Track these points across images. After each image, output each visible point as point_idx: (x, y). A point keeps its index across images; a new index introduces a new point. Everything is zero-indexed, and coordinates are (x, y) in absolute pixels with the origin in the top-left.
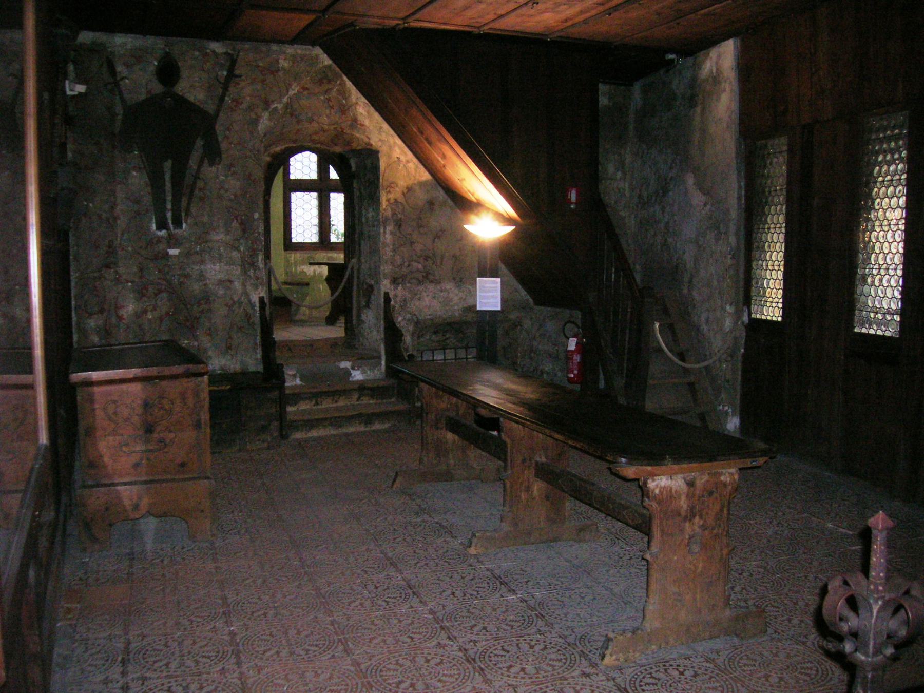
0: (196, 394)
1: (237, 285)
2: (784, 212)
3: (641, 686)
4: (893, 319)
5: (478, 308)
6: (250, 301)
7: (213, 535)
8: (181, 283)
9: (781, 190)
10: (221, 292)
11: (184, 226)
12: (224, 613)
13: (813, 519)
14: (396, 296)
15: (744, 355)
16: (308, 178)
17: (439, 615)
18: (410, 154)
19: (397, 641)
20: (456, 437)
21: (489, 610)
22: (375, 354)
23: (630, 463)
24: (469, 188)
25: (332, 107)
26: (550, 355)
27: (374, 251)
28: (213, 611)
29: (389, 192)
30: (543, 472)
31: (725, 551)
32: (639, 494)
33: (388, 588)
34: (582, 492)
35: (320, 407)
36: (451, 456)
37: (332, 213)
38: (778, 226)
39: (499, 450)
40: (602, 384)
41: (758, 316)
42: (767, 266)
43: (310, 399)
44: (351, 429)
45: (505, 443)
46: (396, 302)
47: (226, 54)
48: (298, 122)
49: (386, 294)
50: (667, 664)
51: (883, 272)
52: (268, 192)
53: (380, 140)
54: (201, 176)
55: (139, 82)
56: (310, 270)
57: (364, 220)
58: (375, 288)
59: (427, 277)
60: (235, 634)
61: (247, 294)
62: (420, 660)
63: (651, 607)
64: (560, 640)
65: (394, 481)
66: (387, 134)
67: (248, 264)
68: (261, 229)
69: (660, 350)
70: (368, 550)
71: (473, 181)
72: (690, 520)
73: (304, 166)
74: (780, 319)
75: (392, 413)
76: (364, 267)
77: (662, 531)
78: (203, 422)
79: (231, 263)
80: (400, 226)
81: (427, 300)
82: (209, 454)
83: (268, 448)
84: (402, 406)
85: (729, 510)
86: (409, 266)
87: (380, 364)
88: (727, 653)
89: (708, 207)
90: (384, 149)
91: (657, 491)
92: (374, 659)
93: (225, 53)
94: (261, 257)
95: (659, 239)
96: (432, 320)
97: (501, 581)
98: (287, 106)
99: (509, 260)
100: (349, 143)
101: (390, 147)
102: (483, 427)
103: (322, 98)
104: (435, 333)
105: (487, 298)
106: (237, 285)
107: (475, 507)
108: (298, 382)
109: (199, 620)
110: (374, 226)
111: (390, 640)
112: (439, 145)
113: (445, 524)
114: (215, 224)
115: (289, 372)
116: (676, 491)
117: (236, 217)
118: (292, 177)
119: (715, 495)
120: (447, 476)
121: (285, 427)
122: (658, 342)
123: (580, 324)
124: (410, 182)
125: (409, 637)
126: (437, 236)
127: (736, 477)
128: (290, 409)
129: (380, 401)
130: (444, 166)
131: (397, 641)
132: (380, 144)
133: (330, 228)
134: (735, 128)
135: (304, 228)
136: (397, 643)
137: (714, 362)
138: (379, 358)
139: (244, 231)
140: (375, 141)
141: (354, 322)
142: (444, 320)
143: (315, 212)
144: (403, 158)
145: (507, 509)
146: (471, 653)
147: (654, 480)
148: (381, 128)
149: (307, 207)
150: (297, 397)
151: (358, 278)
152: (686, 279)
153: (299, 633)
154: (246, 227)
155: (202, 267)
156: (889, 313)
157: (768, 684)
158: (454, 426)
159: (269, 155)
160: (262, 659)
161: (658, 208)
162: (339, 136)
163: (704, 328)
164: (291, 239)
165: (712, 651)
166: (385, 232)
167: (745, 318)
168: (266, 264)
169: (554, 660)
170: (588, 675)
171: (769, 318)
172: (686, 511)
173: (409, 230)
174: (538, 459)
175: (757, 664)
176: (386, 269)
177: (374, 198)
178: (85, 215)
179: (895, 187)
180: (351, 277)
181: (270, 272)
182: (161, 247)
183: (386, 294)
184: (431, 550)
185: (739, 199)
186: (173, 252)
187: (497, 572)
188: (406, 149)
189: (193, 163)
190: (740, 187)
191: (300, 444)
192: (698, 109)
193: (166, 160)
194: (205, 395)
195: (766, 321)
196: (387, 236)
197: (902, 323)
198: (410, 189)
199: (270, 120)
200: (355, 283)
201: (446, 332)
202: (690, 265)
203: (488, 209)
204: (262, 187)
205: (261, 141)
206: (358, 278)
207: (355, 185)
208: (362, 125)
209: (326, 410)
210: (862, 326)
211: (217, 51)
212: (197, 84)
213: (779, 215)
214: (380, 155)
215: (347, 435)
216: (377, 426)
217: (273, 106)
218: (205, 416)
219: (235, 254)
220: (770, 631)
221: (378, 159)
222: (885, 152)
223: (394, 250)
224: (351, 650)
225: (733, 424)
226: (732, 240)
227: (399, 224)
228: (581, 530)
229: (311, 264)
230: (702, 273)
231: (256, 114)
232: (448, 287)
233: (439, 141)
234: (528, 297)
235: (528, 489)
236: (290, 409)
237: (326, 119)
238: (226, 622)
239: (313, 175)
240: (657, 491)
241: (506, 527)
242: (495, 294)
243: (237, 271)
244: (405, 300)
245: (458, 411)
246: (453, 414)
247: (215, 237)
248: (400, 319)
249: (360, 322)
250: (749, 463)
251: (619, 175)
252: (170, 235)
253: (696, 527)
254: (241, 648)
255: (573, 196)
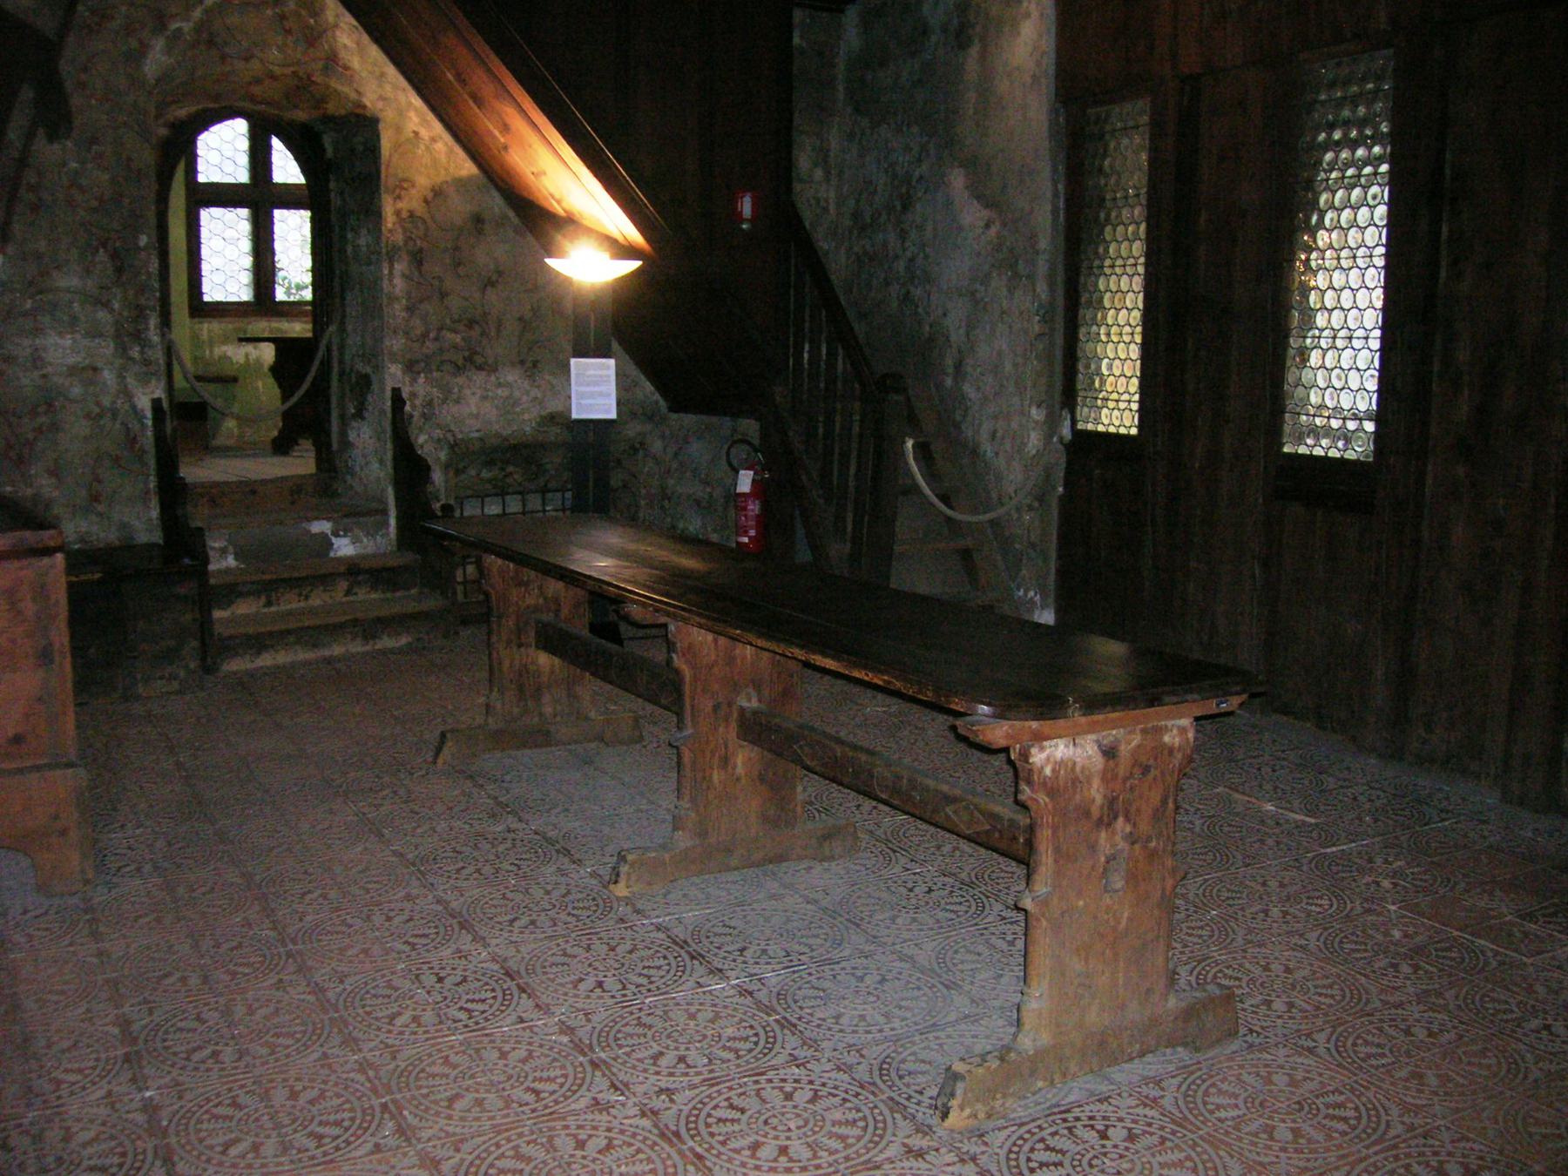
0: (41, 591)
1: (108, 376)
2: (1143, 236)
3: (756, 1035)
4: (1360, 429)
5: (575, 416)
6: (134, 407)
7: (87, 882)
9: (1137, 195)
10: (77, 391)
12: (127, 1058)
13: (1237, 796)
14: (414, 395)
15: (1061, 498)
16: (233, 181)
17: (583, 1034)
18: (438, 127)
19: (508, 1102)
20: (557, 661)
21: (679, 1016)
22: (374, 505)
23: (1000, 715)
24: (552, 190)
25: (288, 32)
26: (698, 503)
27: (373, 310)
28: (103, 1056)
29: (399, 197)
30: (754, 729)
31: (1170, 882)
32: (1011, 774)
33: (465, 980)
34: (849, 773)
35: (273, 609)
36: (546, 698)
37: (278, 246)
38: (1131, 261)
39: (665, 690)
40: (803, 555)
41: (1090, 427)
42: (1108, 335)
43: (256, 594)
44: (337, 650)
45: (677, 672)
46: (413, 407)
48: (223, 58)
49: (396, 393)
50: (1069, 1116)
51: (1340, 343)
52: (163, 199)
53: (382, 98)
56: (238, 354)
57: (349, 249)
58: (374, 378)
59: (472, 361)
60: (157, 1108)
61: (129, 396)
62: (565, 1144)
63: (1034, 1005)
64: (841, 1076)
65: (438, 751)
66: (396, 87)
67: (129, 334)
68: (154, 266)
69: (916, 489)
70: (408, 898)
71: (565, 179)
72: (1109, 825)
73: (223, 151)
74: (1134, 431)
75: (414, 617)
76: (353, 341)
77: (1057, 850)
78: (57, 646)
79: (94, 333)
80: (420, 263)
81: (472, 404)
82: (71, 710)
83: (179, 692)
84: (433, 603)
85: (1175, 801)
86: (436, 339)
87: (387, 524)
88: (1175, 1081)
89: (993, 230)
90: (388, 116)
91: (1048, 771)
92: (466, 1147)
94: (153, 321)
95: (895, 289)
96: (481, 439)
97: (690, 951)
98: (200, 27)
99: (625, 325)
100: (320, 102)
101: (401, 113)
102: (602, 637)
103: (269, 12)
104: (490, 463)
105: (592, 395)
106: (108, 376)
107: (615, 796)
108: (231, 561)
109: (72, 1077)
110: (369, 264)
111: (492, 1099)
112: (498, 105)
113: (550, 834)
115: (215, 543)
116: (1083, 768)
117: (104, 245)
118: (202, 179)
119: (1153, 772)
120: (541, 737)
121: (212, 649)
122: (913, 479)
123: (756, 442)
124: (439, 180)
125: (528, 1089)
126: (491, 283)
127: (1191, 735)
128: (218, 614)
129: (389, 595)
130: (506, 148)
131: (508, 1102)
132: (380, 105)
133: (274, 275)
134: (1047, 86)
135: (225, 268)
136: (508, 1107)
137: (1008, 514)
138: (385, 512)
139: (119, 270)
140: (370, 100)
141: (335, 446)
142: (506, 439)
143: (246, 245)
144: (424, 133)
145: (685, 804)
146: (668, 1118)
147: (1042, 749)
148: (383, 75)
149: (229, 233)
150: (231, 591)
151: (341, 362)
152: (949, 362)
153: (294, 1095)
154: (121, 264)
156: (1355, 417)
157: (1276, 1146)
158: (553, 640)
159: (165, 125)
160: (221, 1164)
161: (892, 237)
162: (302, 88)
163: (987, 448)
164: (201, 294)
165: (1146, 1080)
166: (391, 273)
167: (1066, 432)
168: (163, 335)
169: (840, 1123)
170: (920, 1154)
171: (1112, 429)
172: (1102, 807)
173: (437, 270)
174: (745, 704)
175: (1240, 1102)
176: (395, 343)
177: (372, 212)
179: (1366, 188)
180: (326, 365)
181: (170, 350)
183: (396, 393)
184: (537, 893)
185: (1055, 212)
187: (679, 932)
188: (430, 116)
190: (1056, 195)
191: (245, 683)
192: (974, 51)
194: (60, 596)
195: (1107, 435)
196: (396, 280)
197: (1378, 436)
198: (438, 192)
199: (168, 51)
200: (336, 370)
201: (508, 462)
202: (957, 336)
203: (589, 231)
204: (150, 187)
205: (150, 93)
206: (341, 362)
207: (332, 185)
208: (346, 68)
209: (290, 613)
210: (1300, 440)
213: (1131, 242)
214: (381, 126)
215: (329, 661)
216: (387, 642)
217: (174, 26)
218: (60, 636)
219: (102, 315)
220: (1243, 1031)
221: (377, 136)
222: (1347, 124)
223: (410, 309)
224: (413, 1129)
225: (1047, 617)
226: (1042, 288)
227: (418, 259)
228: (827, 837)
229: (241, 340)
230: (983, 351)
231: (141, 42)
232: (510, 378)
233: (497, 97)
234: (657, 396)
235: (725, 762)
236: (218, 614)
237: (276, 56)
238: (134, 1080)
239: (240, 174)
240: (1048, 771)
241: (683, 840)
242: (603, 388)
243: (107, 348)
244: (430, 403)
245: (557, 612)
246: (547, 617)
247: (63, 282)
248: (422, 439)
249: (346, 444)
250: (1211, 707)
251: (819, 174)
253: (1118, 838)
254: (173, 1140)
255: (746, 207)
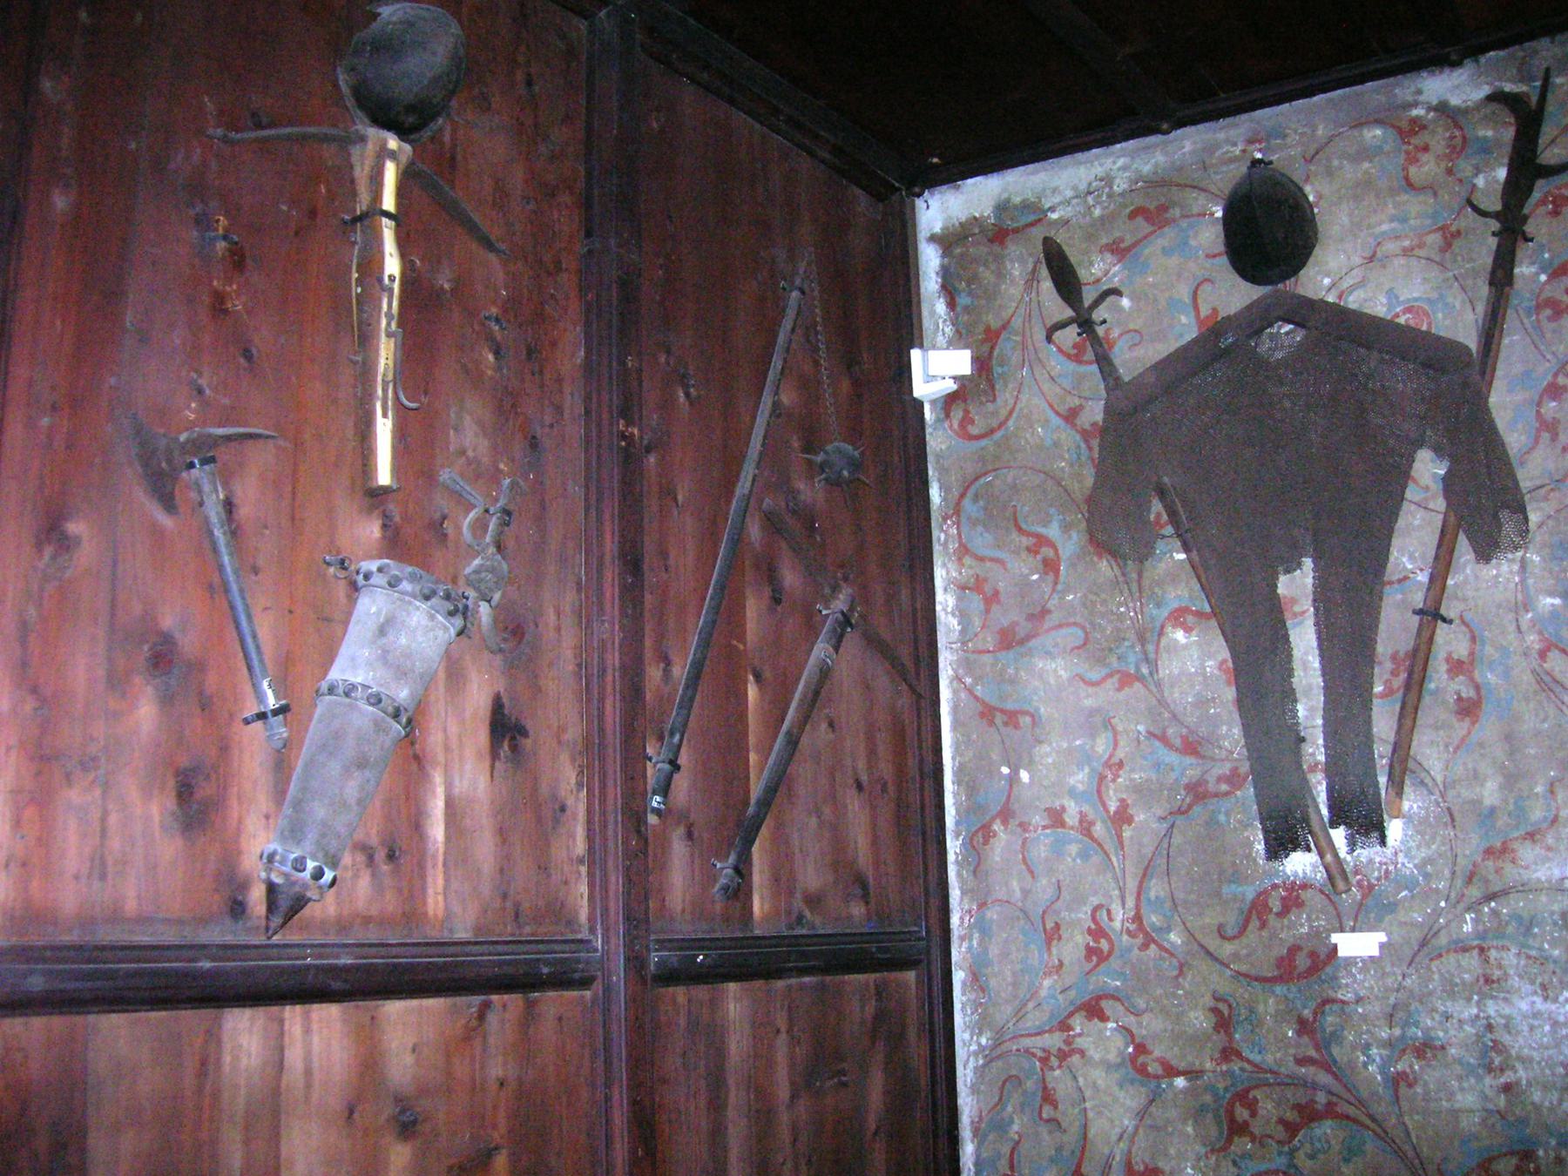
8: (1398, 1081)
11: (1395, 830)
47: (1497, 97)
54: (1449, 609)
55: (1174, 291)
93: (1491, 98)
114: (1537, 814)
155: (1491, 1008)
178: (1005, 815)
182: (1302, 925)
186: (1356, 945)
189: (1410, 551)
193: (1292, 566)
211: (1455, 101)
212: (1391, 247)
252: (1336, 872)
255: (935, 160)
